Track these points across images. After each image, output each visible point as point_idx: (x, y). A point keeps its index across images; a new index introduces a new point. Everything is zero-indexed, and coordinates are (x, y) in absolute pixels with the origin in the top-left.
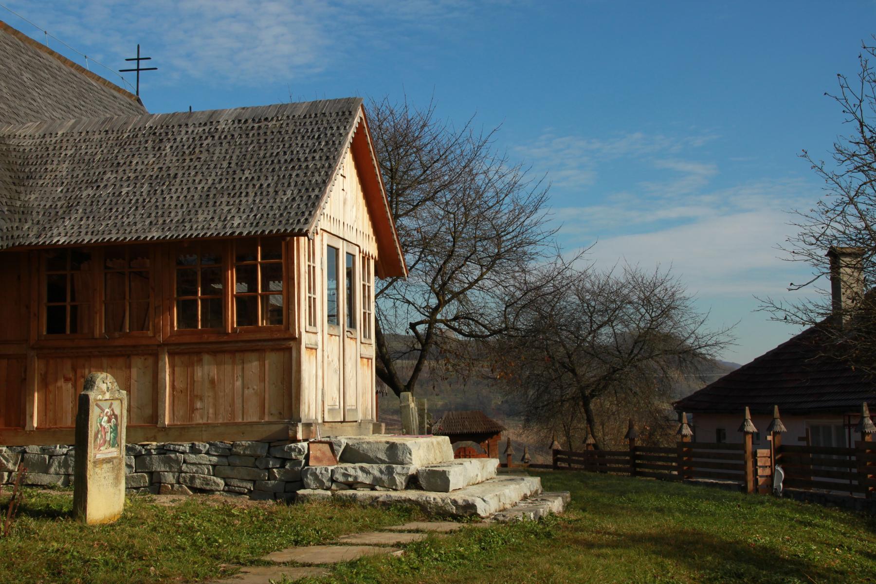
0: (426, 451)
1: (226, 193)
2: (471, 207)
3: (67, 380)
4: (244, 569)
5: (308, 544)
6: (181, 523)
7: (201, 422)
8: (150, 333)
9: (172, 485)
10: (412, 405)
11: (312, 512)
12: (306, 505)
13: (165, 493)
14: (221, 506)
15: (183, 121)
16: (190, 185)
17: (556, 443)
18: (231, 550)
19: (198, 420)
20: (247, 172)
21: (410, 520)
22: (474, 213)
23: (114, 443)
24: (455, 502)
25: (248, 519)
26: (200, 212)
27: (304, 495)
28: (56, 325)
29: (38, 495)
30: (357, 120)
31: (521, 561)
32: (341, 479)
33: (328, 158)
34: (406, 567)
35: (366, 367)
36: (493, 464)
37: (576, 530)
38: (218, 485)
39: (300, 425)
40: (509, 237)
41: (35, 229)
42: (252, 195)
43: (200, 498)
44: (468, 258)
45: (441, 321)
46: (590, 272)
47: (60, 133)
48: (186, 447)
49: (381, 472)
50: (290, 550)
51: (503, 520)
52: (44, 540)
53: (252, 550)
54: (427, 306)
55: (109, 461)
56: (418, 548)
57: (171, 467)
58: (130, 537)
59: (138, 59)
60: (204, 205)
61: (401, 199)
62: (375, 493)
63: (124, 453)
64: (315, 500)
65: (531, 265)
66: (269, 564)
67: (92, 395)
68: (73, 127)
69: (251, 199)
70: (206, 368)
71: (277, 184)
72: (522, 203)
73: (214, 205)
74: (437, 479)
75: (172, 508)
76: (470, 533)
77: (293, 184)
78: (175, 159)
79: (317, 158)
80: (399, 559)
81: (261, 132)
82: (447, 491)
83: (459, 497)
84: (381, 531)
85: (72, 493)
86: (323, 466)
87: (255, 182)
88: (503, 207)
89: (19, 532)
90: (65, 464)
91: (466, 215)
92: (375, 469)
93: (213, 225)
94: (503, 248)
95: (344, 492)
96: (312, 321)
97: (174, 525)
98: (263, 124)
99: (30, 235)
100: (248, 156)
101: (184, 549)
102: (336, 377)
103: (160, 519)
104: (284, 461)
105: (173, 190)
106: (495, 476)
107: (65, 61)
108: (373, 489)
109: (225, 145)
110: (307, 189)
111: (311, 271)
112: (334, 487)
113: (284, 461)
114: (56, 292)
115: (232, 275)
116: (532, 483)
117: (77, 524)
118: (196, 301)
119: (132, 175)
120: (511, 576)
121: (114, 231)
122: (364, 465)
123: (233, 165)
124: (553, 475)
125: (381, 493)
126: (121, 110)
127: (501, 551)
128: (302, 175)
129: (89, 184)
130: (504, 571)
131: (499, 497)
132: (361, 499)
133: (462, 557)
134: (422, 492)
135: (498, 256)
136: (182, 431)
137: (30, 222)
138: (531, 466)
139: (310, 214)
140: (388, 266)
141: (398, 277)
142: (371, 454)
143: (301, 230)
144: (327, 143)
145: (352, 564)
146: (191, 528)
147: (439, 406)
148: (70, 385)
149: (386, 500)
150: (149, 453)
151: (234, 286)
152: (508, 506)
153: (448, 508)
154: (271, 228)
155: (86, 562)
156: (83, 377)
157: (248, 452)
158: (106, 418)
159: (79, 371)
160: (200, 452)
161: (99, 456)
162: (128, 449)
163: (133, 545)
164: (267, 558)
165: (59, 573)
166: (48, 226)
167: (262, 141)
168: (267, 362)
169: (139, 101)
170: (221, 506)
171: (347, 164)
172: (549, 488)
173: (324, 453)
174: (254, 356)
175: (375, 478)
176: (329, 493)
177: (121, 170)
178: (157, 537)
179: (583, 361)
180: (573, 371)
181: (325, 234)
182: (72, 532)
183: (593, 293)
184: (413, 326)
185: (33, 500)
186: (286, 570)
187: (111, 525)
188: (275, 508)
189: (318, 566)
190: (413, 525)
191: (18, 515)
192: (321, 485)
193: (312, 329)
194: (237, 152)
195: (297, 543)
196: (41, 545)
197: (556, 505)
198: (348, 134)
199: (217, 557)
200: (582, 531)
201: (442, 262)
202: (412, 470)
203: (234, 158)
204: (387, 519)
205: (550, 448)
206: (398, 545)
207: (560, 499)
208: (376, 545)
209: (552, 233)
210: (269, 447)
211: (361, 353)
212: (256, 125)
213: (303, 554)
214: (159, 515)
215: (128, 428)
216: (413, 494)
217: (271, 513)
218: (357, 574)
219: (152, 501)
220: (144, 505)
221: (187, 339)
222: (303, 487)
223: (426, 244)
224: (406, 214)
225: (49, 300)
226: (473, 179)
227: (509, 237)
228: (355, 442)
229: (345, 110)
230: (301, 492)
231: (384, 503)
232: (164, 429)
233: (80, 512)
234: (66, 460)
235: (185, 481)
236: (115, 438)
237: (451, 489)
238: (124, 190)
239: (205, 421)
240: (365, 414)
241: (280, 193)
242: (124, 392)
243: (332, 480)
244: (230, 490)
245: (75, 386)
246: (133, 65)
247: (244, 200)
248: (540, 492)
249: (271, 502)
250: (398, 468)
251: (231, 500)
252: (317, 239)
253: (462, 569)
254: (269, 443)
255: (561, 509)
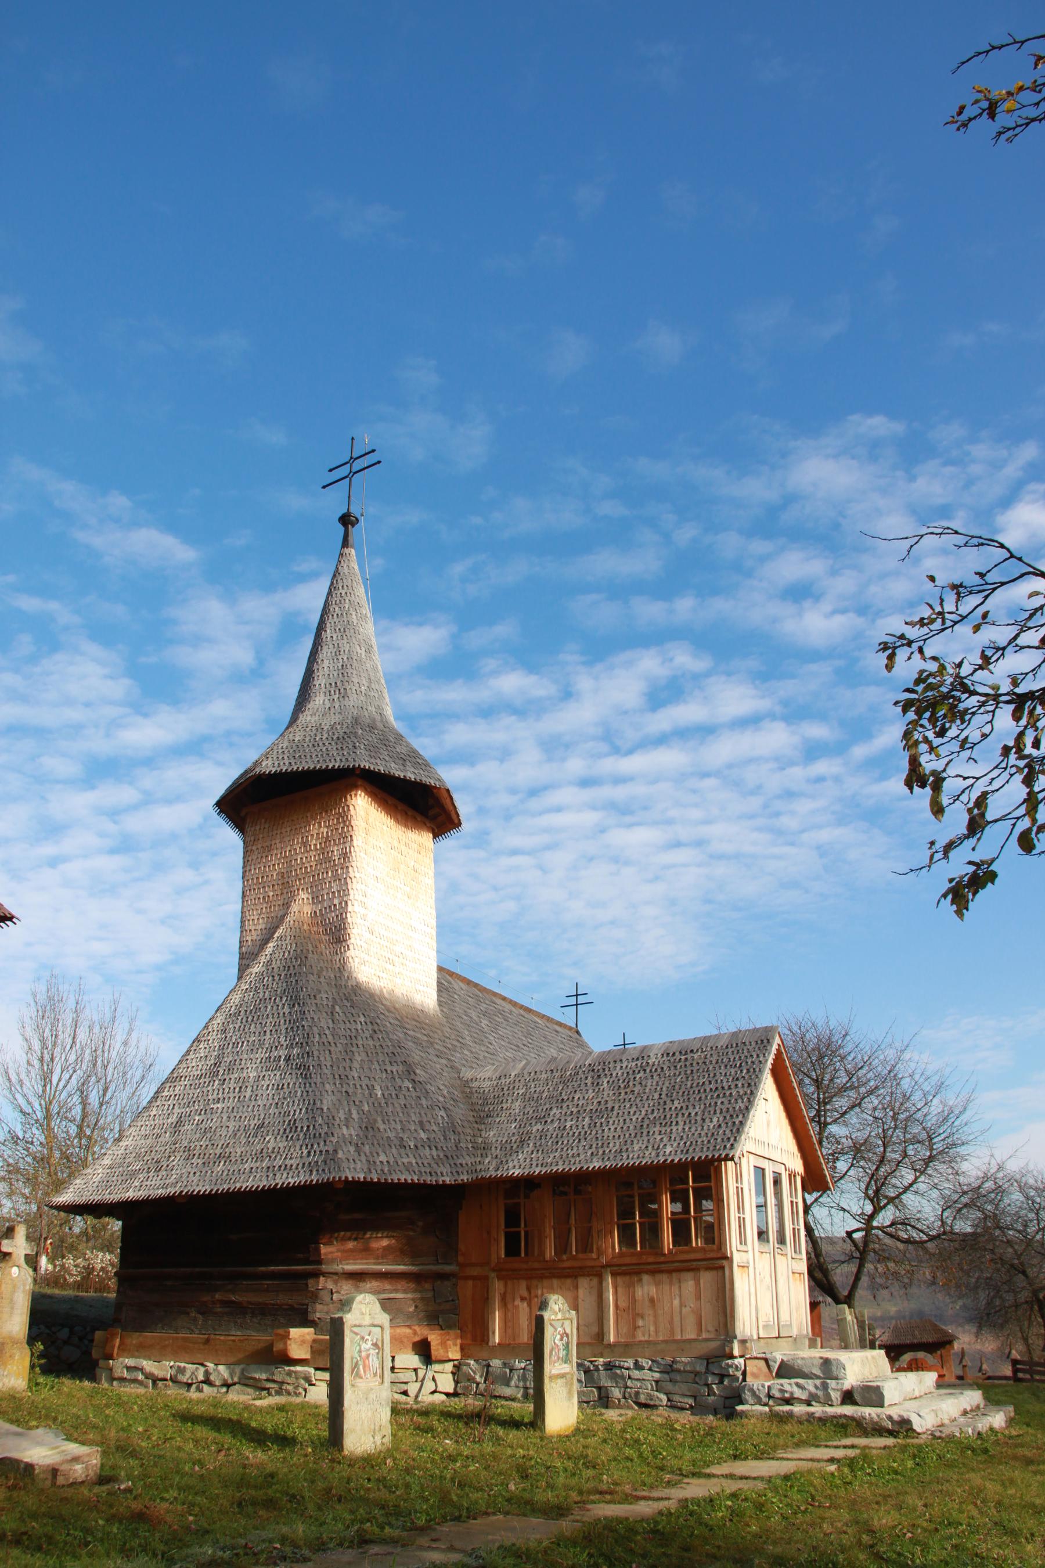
0: (861, 1366)
1: (658, 1123)
2: (898, 1116)
3: (523, 1299)
4: (686, 1480)
5: (746, 1458)
6: (628, 1436)
7: (643, 1339)
8: (594, 1255)
9: (619, 1400)
10: (849, 1318)
11: (751, 1427)
12: (745, 1421)
13: (613, 1408)
14: (664, 1421)
15: (618, 1058)
16: (626, 1117)
17: (1014, 1352)
18: (675, 1463)
19: (640, 1337)
20: (676, 1102)
21: (846, 1436)
22: (902, 1117)
23: (567, 1360)
24: (890, 1418)
25: (690, 1434)
26: (635, 1141)
27: (743, 1411)
28: (512, 1249)
29: (502, 1406)
30: (775, 1047)
31: (955, 1477)
32: (778, 1395)
33: (749, 1085)
34: (839, 1482)
35: (798, 1282)
36: (931, 1377)
37: (1016, 1446)
38: (661, 1400)
39: (736, 1342)
40: (940, 1138)
41: (494, 1163)
42: (681, 1123)
43: (644, 1413)
44: (900, 1162)
45: (878, 1228)
46: (1031, 1167)
47: (513, 1074)
48: (630, 1363)
49: (816, 1387)
50: (729, 1464)
51: (939, 1438)
52: (512, 1447)
53: (694, 1462)
54: (863, 1213)
55: (562, 1376)
56: (851, 1463)
57: (617, 1383)
58: (584, 1447)
59: (577, 995)
60: (639, 1135)
61: (828, 1107)
62: (811, 1409)
63: (575, 1369)
64: (752, 1416)
65: (965, 1166)
66: (709, 1476)
67: (547, 1315)
68: (524, 1068)
69: (680, 1128)
70: (646, 1288)
71: (703, 1112)
72: (951, 1103)
73: (648, 1135)
74: (872, 1395)
75: (619, 1422)
76: (904, 1448)
77: (718, 1112)
78: (611, 1093)
79: (740, 1085)
80: (832, 1474)
81: (688, 1063)
82: (882, 1406)
83: (895, 1413)
84: (818, 1446)
85: (532, 1405)
86: (759, 1381)
87: (683, 1111)
88: (932, 1108)
89: (491, 1439)
90: (524, 1378)
91: (894, 1118)
92: (810, 1385)
93: (647, 1153)
94: (935, 1152)
95: (781, 1408)
96: (743, 1240)
97: (622, 1438)
98: (689, 1056)
99: (490, 1169)
100: (677, 1087)
101: (632, 1460)
102: (768, 1294)
103: (609, 1432)
104: (722, 1377)
105: (611, 1122)
106: (933, 1390)
107: (514, 1004)
108: (809, 1404)
109: (656, 1078)
110: (731, 1116)
111: (740, 1192)
112: (771, 1403)
113: (722, 1377)
114: (512, 1218)
115: (666, 1198)
116: (973, 1397)
117: (538, 1434)
118: (635, 1224)
119: (575, 1110)
120: (941, 1491)
121: (561, 1163)
122: (800, 1381)
123: (663, 1096)
124: (994, 1391)
125: (817, 1409)
126: (562, 1043)
127: (935, 1467)
128: (726, 1102)
129: (538, 1119)
130: (937, 1488)
131: (935, 1412)
132: (798, 1414)
133: (896, 1472)
134: (857, 1408)
135: (931, 1158)
136: (626, 1347)
137: (490, 1157)
138: (989, 1378)
139: (735, 1140)
140: (815, 1180)
141: (824, 1192)
142: (806, 1370)
143: (727, 1155)
144: (748, 1070)
145: (786, 1478)
146: (637, 1441)
147: (892, 1313)
148: (525, 1304)
149: (822, 1415)
150: (597, 1369)
151: (669, 1207)
152: (946, 1421)
153: (884, 1424)
154: (700, 1154)
155: (548, 1468)
156: (537, 1296)
157: (688, 1368)
158: (558, 1337)
159: (533, 1291)
160: (643, 1368)
161: (554, 1372)
162: (579, 1365)
163: (587, 1455)
164: (708, 1471)
165: (527, 1476)
166: (504, 1160)
167: (689, 1072)
168: (702, 1281)
169: (578, 1032)
170: (664, 1421)
171: (768, 1087)
172: (993, 1400)
173: (760, 1369)
174: (689, 1275)
175: (811, 1394)
176: (767, 1409)
177: (565, 1105)
178: (608, 1448)
179: (1035, 1261)
180: (1024, 1273)
181: (751, 1156)
182: (534, 1440)
183: (1036, 1189)
184: (849, 1234)
185: (499, 1410)
186: (725, 1483)
187: (567, 1436)
188: (714, 1424)
189: (754, 1478)
190: (848, 1441)
191: (488, 1424)
192: (759, 1401)
193: (743, 1248)
194: (667, 1084)
195: (735, 1457)
196: (509, 1452)
197: (998, 1419)
198: (766, 1061)
199: (662, 1469)
200: (1022, 1446)
201: (874, 1167)
202: (847, 1385)
203: (664, 1089)
204: (823, 1435)
205: (1008, 1357)
206: (832, 1460)
207: (1002, 1413)
208: (812, 1460)
209: (983, 1132)
210: (708, 1363)
211: (794, 1265)
212: (683, 1057)
213: (741, 1468)
214: (609, 1428)
215: (578, 1344)
216: (848, 1410)
217: (711, 1428)
218: (791, 1486)
219: (601, 1414)
220: (594, 1418)
221: (627, 1260)
222: (741, 1403)
223: (858, 1150)
224: (835, 1121)
225: (506, 1227)
226: (898, 1084)
227: (940, 1138)
228: (790, 1357)
229: (763, 1038)
230: (739, 1408)
231: (820, 1419)
232: (609, 1345)
233: (539, 1423)
234: (524, 1375)
235: (630, 1396)
236: (567, 1355)
237: (886, 1403)
238: (568, 1124)
239: (646, 1338)
240: (800, 1329)
241: (707, 1121)
242: (574, 1312)
243: (770, 1396)
244: (672, 1406)
245: (529, 1305)
246: (573, 1001)
247: (674, 1128)
248: (982, 1406)
249: (711, 1417)
250: (832, 1383)
251: (674, 1415)
252: (744, 1161)
253: (895, 1484)
254: (708, 1359)
255: (1003, 1424)
